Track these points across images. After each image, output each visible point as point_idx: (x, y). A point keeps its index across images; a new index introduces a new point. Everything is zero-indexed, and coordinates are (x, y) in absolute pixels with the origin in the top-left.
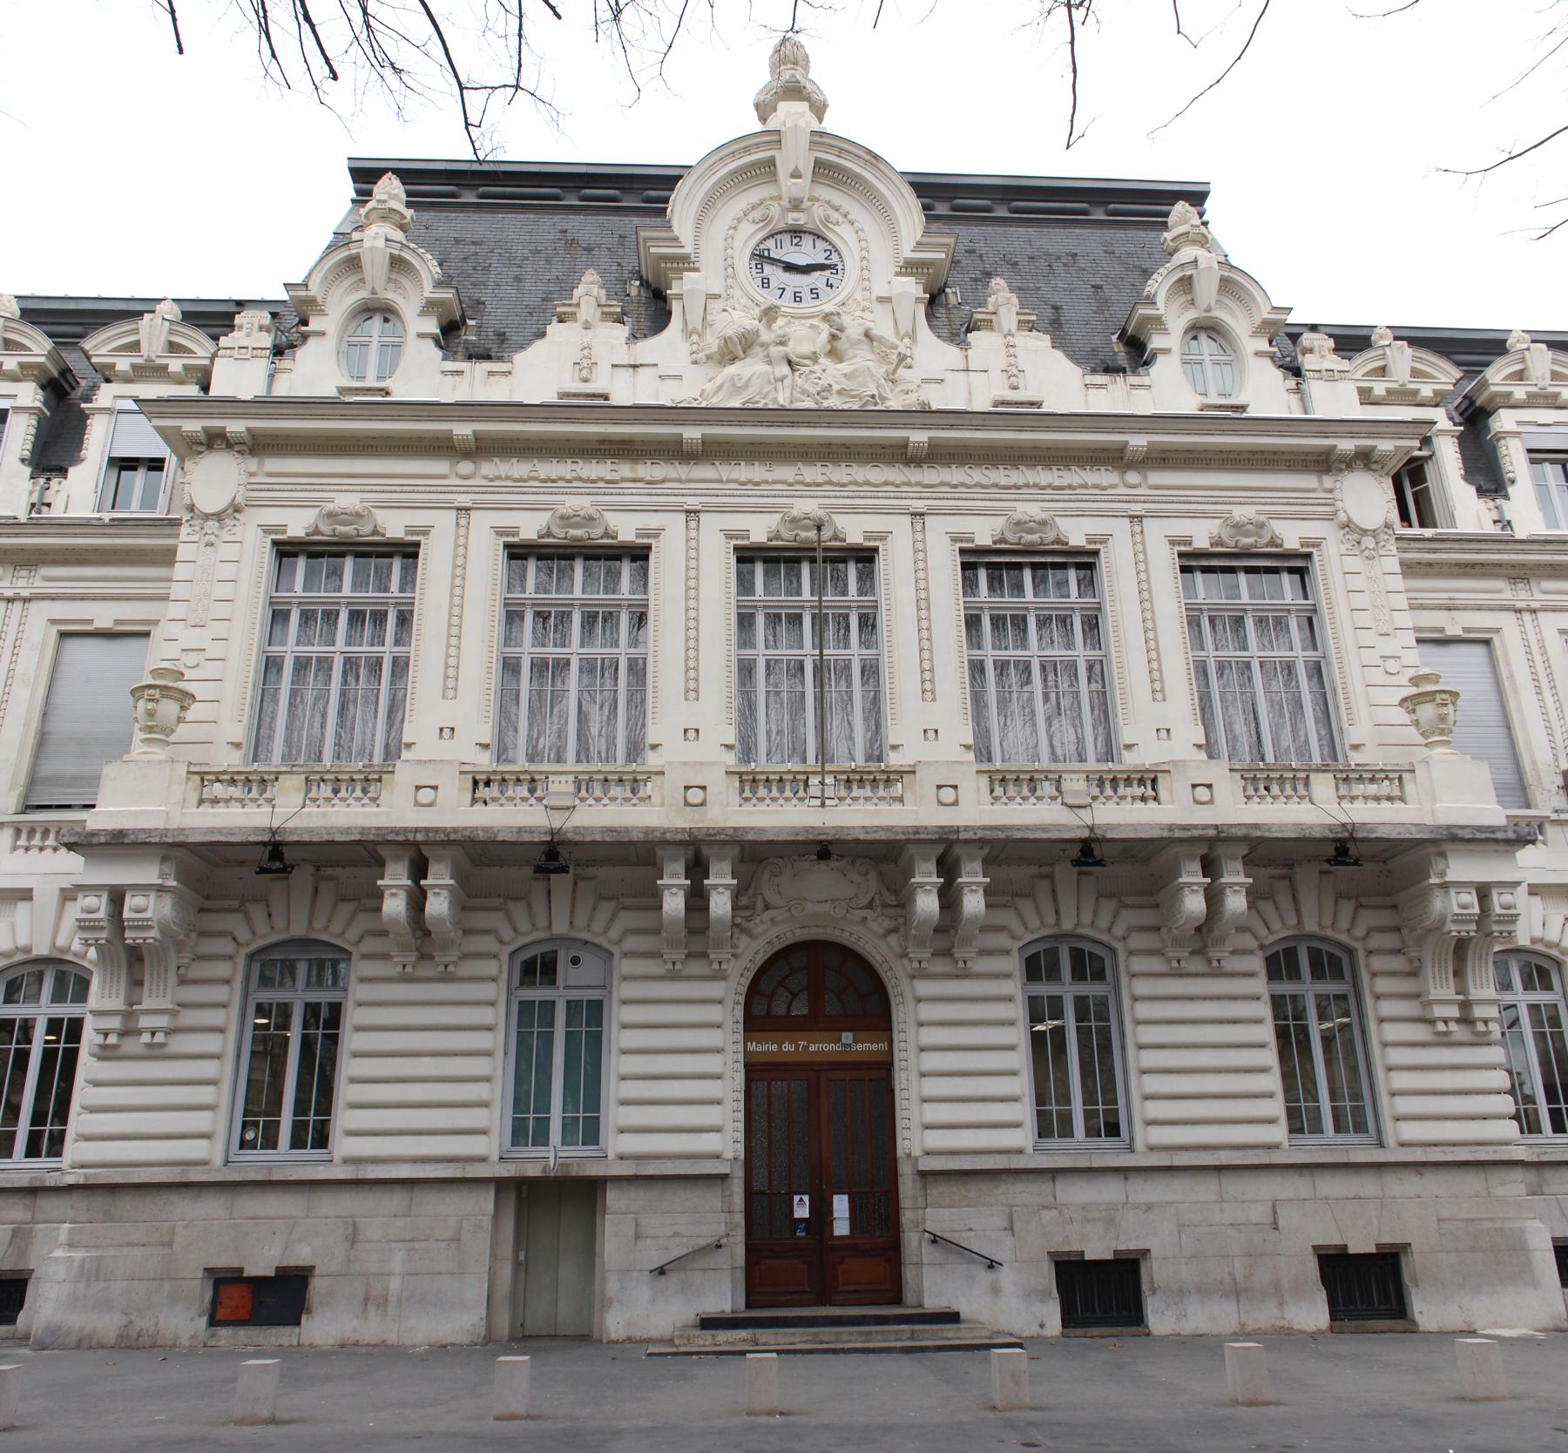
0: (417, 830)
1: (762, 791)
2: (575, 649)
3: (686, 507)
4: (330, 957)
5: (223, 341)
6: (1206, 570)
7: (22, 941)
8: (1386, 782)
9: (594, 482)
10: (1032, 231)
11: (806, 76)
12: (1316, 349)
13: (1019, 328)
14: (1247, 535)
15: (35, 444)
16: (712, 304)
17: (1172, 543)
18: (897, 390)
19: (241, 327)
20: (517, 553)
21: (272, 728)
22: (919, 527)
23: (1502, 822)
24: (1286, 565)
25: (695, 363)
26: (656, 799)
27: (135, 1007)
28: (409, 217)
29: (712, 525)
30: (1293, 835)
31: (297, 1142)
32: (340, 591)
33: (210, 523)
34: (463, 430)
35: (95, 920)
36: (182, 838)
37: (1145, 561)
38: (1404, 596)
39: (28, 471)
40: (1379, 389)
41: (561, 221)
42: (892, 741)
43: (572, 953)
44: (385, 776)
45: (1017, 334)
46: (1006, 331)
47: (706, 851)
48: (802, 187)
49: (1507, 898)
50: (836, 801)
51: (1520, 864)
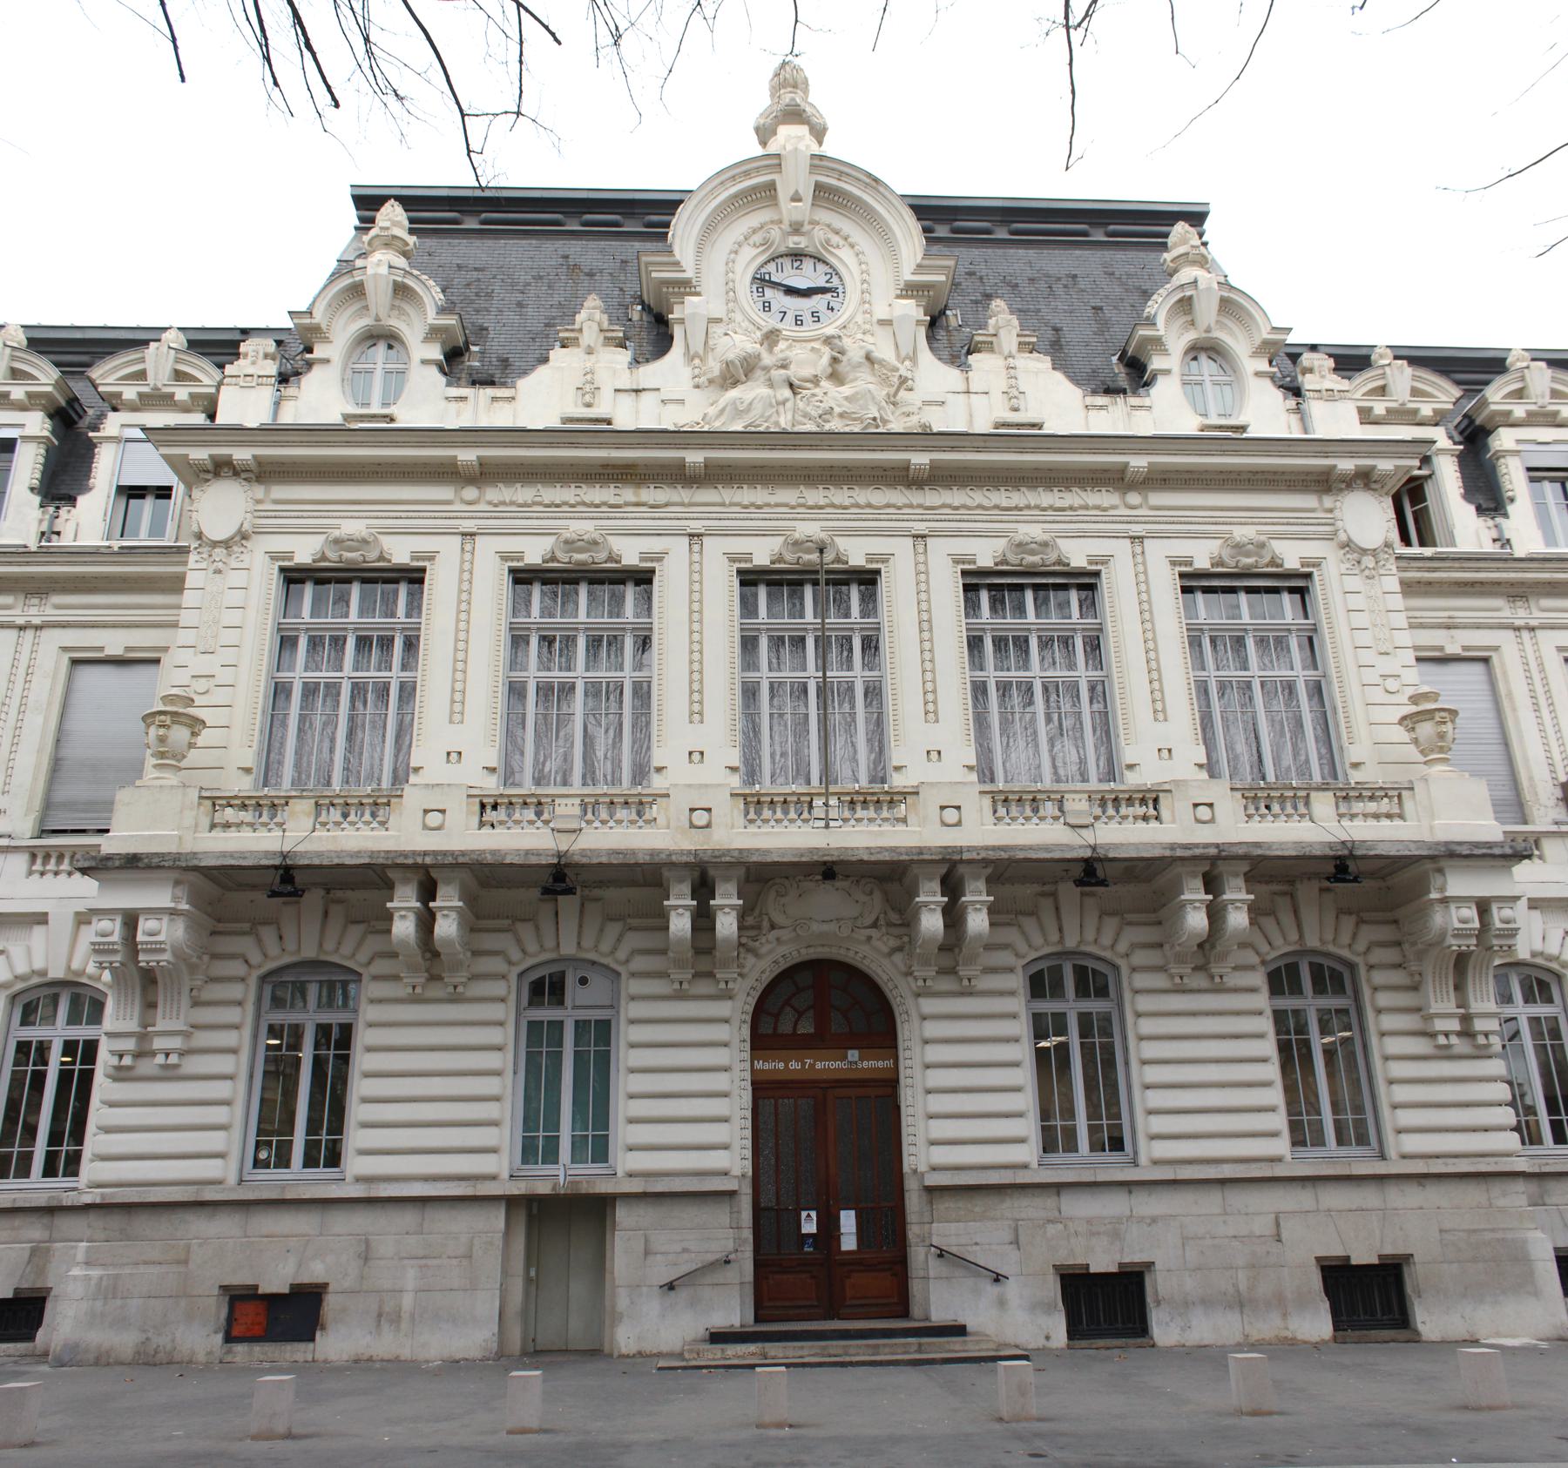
0: (425, 853)
1: (767, 813)
3: (689, 531)
5: (229, 369)
6: (1207, 590)
7: (38, 964)
9: (597, 506)
10: (1031, 253)
11: (805, 100)
12: (1316, 369)
13: (1020, 350)
14: (1248, 555)
15: (43, 473)
20: (522, 577)
21: (281, 753)
22: (921, 549)
23: (1499, 837)
25: (697, 387)
26: (661, 821)
27: (150, 1029)
28: (411, 244)
29: (715, 548)
31: (310, 1161)
34: (467, 456)
35: (109, 943)
36: (195, 862)
37: (1146, 582)
38: (1404, 615)
39: (37, 499)
40: (1379, 408)
42: (895, 763)
43: (580, 974)
44: (393, 800)
45: (1018, 355)
46: (1006, 353)
47: (712, 872)
48: (802, 210)
49: (1507, 913)
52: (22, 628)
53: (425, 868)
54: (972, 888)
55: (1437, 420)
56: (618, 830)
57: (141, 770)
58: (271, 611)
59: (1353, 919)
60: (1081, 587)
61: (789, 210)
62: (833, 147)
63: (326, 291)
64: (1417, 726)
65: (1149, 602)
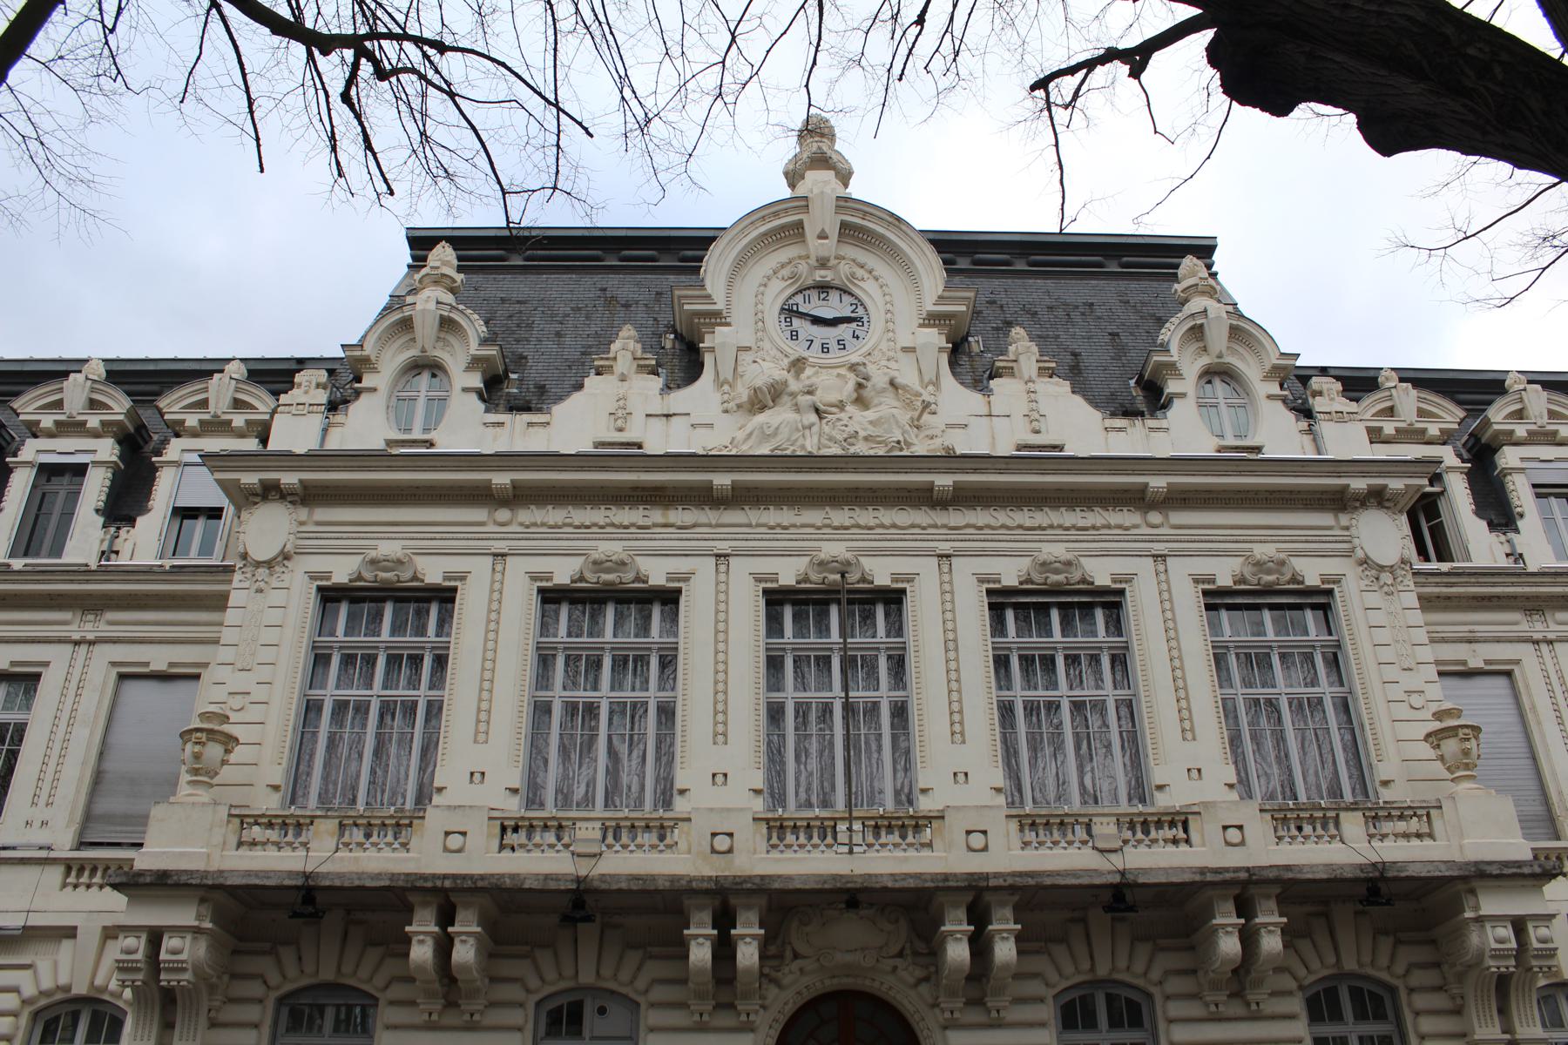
0: (445, 877)
1: (790, 838)
3: (716, 551)
5: (283, 398)
7: (63, 980)
8: (1415, 819)
9: (626, 527)
11: (831, 147)
12: (1325, 392)
13: (1040, 375)
14: (1269, 572)
15: (109, 495)
16: (743, 356)
17: (1196, 581)
18: (922, 435)
20: (551, 597)
21: (310, 766)
22: (723, 568)
23: (1529, 856)
25: (726, 411)
26: (682, 845)
28: (459, 281)
29: (741, 569)
30: (1325, 876)
32: (379, 636)
34: (501, 479)
35: (133, 961)
36: (221, 881)
37: (1171, 600)
38: (1423, 630)
39: (101, 520)
41: (600, 280)
42: (922, 785)
43: (599, 1003)
44: (415, 822)
46: (1026, 378)
47: (733, 901)
48: (829, 247)
49: (1543, 932)
50: (865, 848)
51: (1547, 897)
52: (77, 643)
54: (998, 916)
55: (1445, 439)
56: (639, 855)
57: (176, 784)
58: (307, 630)
59: (1391, 939)
61: (816, 247)
62: (856, 190)
63: (377, 326)
64: (1441, 743)
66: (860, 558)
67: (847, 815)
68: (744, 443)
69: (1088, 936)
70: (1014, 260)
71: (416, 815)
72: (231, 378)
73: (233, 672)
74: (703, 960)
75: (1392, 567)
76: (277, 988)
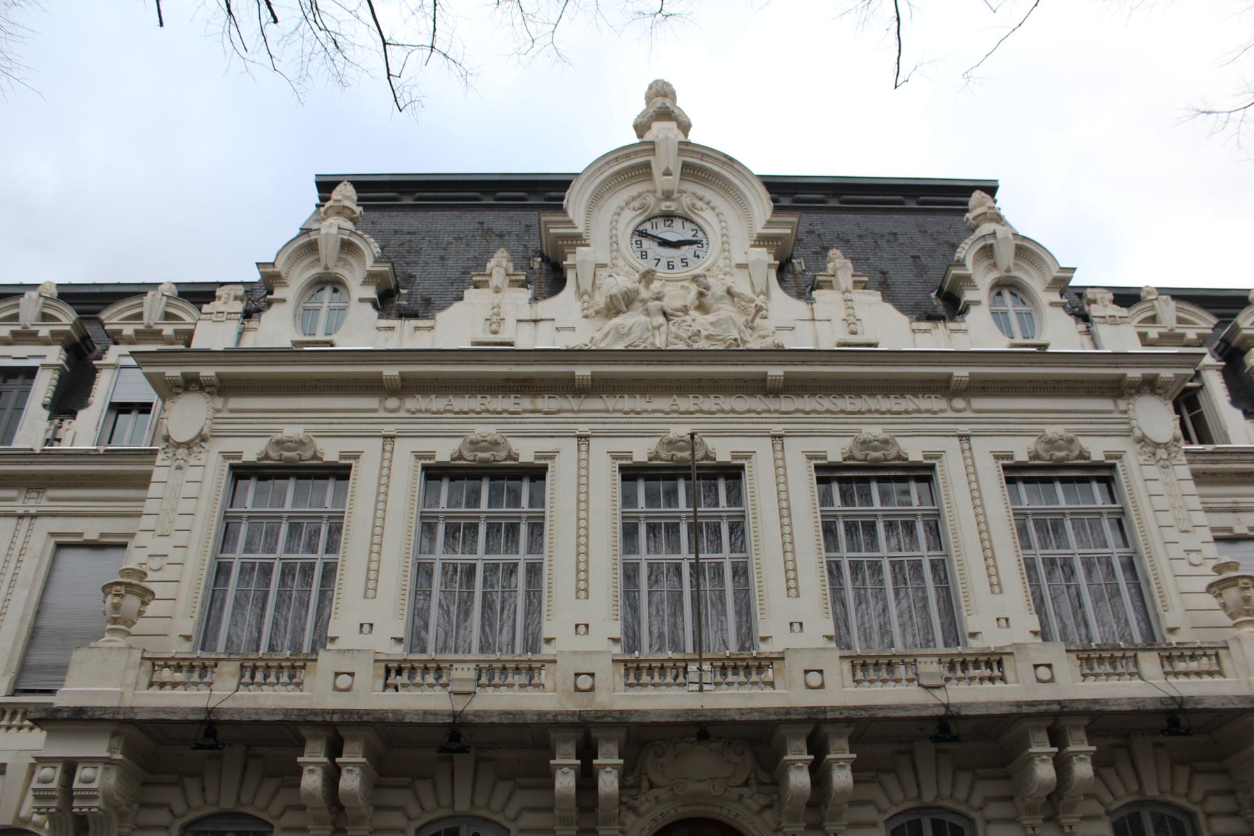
0: (334, 712)
1: (645, 678)
2: (480, 556)
3: (578, 433)
4: (255, 829)
6: (1027, 481)
10: (859, 217)
12: (1099, 300)
13: (855, 287)
14: (1060, 449)
15: (55, 393)
16: (600, 272)
17: (997, 457)
19: (220, 298)
22: (778, 447)
24: (1095, 474)
25: (586, 317)
29: (600, 448)
30: (1129, 708)
32: (283, 507)
33: (180, 450)
34: (391, 372)
35: (48, 790)
36: (132, 716)
37: (975, 473)
39: (47, 413)
40: (1153, 333)
42: (762, 634)
44: (309, 664)
45: (853, 291)
46: (844, 289)
47: (595, 734)
48: (673, 182)
52: (21, 517)
53: (333, 725)
55: (1202, 340)
58: (219, 502)
60: (919, 479)
61: (661, 183)
63: (287, 248)
64: (1223, 592)
65: (979, 490)
66: (704, 439)
67: (697, 657)
68: (600, 342)
69: (914, 766)
70: (828, 199)
71: (309, 657)
72: (163, 295)
73: (154, 537)
74: (568, 787)
75: (1166, 444)
76: (183, 816)
